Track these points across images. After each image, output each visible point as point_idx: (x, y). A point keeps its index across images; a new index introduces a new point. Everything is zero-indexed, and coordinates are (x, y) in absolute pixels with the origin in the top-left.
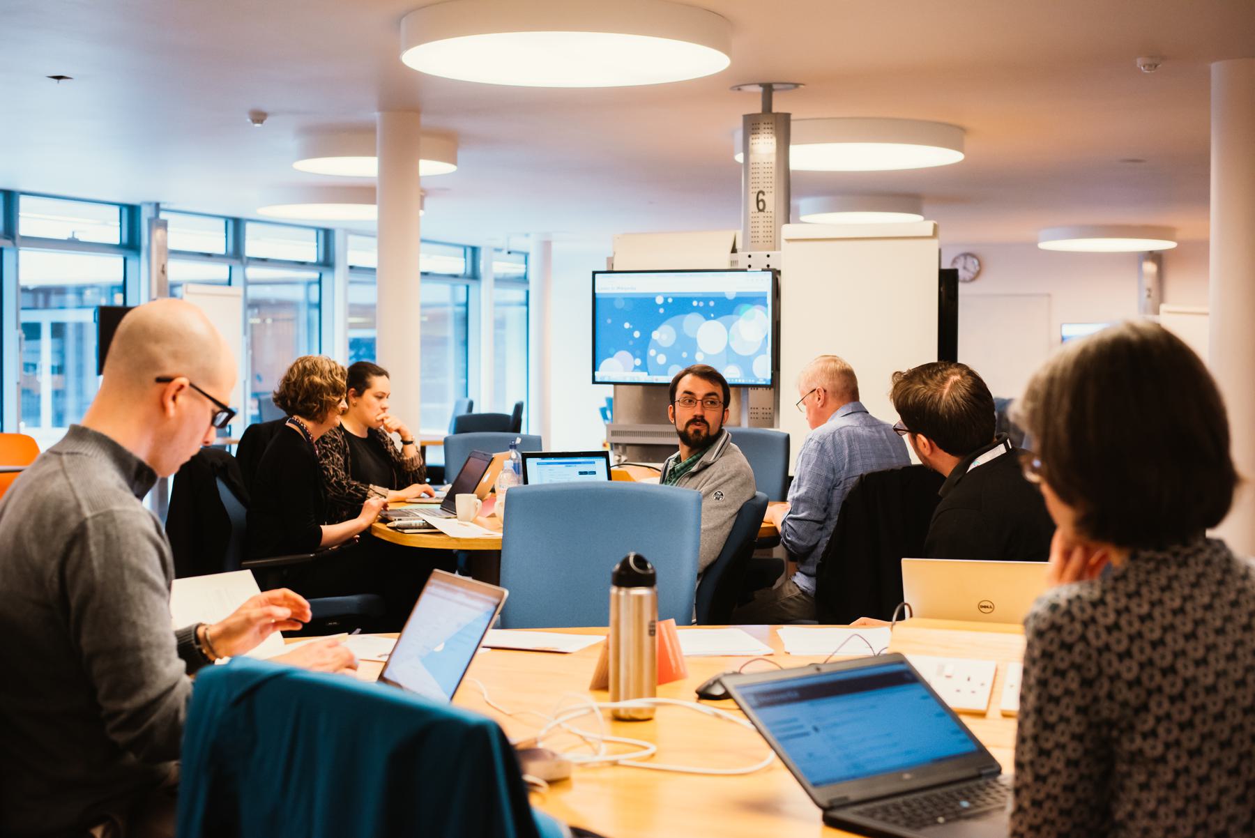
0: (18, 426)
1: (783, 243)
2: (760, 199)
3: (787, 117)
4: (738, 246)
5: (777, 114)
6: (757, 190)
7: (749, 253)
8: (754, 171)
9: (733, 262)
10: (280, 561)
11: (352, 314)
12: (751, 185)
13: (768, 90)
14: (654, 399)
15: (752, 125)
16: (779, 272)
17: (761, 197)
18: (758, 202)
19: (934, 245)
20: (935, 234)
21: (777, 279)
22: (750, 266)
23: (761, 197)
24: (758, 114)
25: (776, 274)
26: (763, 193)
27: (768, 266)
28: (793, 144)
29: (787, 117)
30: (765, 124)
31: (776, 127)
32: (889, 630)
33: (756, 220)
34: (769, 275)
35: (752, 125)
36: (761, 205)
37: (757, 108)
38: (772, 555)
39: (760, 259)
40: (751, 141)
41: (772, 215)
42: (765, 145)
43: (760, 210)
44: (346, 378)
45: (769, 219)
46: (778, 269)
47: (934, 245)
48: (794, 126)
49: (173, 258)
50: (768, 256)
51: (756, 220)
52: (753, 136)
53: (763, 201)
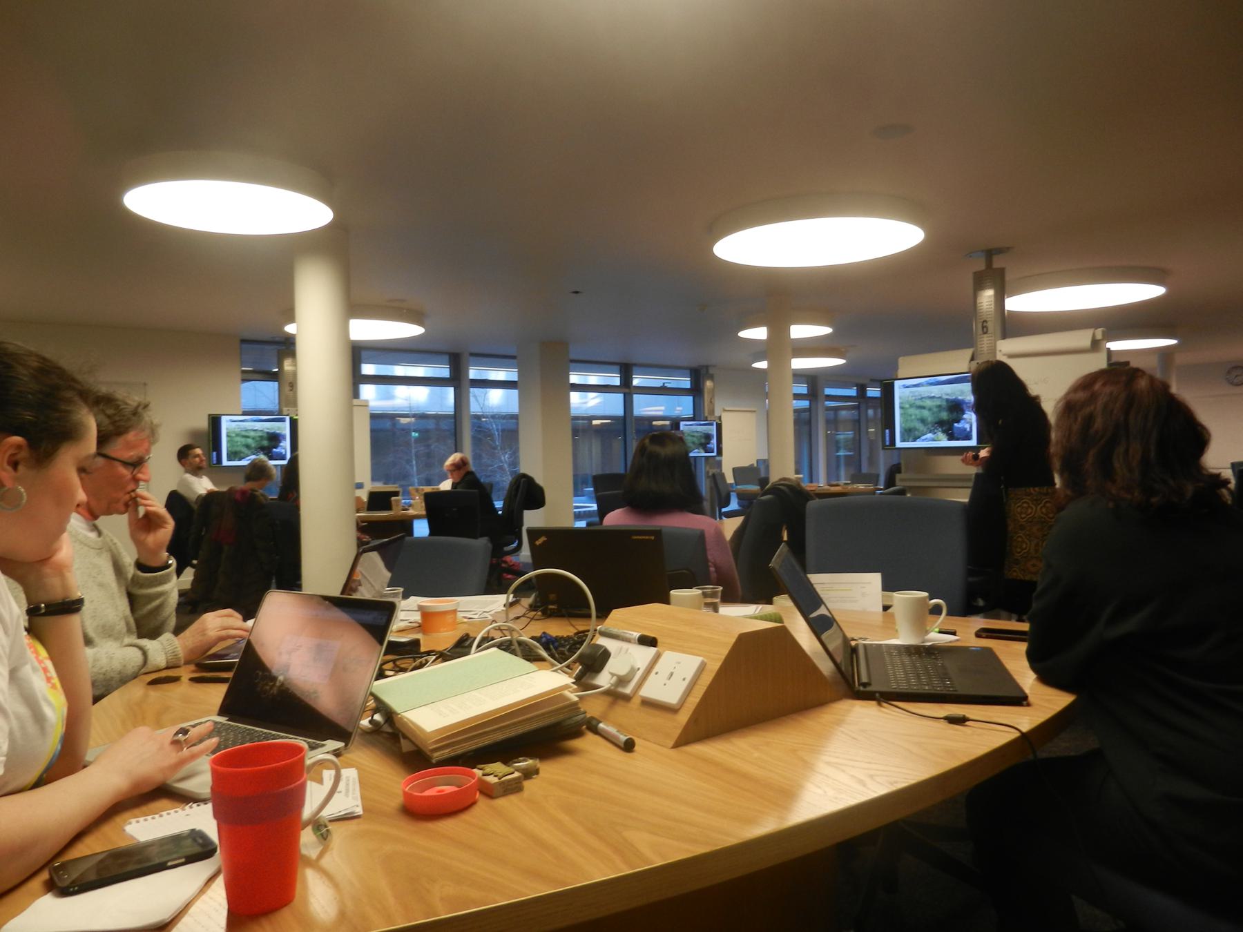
6: (982, 320)
35: (979, 284)
36: (985, 329)
53: (986, 327)
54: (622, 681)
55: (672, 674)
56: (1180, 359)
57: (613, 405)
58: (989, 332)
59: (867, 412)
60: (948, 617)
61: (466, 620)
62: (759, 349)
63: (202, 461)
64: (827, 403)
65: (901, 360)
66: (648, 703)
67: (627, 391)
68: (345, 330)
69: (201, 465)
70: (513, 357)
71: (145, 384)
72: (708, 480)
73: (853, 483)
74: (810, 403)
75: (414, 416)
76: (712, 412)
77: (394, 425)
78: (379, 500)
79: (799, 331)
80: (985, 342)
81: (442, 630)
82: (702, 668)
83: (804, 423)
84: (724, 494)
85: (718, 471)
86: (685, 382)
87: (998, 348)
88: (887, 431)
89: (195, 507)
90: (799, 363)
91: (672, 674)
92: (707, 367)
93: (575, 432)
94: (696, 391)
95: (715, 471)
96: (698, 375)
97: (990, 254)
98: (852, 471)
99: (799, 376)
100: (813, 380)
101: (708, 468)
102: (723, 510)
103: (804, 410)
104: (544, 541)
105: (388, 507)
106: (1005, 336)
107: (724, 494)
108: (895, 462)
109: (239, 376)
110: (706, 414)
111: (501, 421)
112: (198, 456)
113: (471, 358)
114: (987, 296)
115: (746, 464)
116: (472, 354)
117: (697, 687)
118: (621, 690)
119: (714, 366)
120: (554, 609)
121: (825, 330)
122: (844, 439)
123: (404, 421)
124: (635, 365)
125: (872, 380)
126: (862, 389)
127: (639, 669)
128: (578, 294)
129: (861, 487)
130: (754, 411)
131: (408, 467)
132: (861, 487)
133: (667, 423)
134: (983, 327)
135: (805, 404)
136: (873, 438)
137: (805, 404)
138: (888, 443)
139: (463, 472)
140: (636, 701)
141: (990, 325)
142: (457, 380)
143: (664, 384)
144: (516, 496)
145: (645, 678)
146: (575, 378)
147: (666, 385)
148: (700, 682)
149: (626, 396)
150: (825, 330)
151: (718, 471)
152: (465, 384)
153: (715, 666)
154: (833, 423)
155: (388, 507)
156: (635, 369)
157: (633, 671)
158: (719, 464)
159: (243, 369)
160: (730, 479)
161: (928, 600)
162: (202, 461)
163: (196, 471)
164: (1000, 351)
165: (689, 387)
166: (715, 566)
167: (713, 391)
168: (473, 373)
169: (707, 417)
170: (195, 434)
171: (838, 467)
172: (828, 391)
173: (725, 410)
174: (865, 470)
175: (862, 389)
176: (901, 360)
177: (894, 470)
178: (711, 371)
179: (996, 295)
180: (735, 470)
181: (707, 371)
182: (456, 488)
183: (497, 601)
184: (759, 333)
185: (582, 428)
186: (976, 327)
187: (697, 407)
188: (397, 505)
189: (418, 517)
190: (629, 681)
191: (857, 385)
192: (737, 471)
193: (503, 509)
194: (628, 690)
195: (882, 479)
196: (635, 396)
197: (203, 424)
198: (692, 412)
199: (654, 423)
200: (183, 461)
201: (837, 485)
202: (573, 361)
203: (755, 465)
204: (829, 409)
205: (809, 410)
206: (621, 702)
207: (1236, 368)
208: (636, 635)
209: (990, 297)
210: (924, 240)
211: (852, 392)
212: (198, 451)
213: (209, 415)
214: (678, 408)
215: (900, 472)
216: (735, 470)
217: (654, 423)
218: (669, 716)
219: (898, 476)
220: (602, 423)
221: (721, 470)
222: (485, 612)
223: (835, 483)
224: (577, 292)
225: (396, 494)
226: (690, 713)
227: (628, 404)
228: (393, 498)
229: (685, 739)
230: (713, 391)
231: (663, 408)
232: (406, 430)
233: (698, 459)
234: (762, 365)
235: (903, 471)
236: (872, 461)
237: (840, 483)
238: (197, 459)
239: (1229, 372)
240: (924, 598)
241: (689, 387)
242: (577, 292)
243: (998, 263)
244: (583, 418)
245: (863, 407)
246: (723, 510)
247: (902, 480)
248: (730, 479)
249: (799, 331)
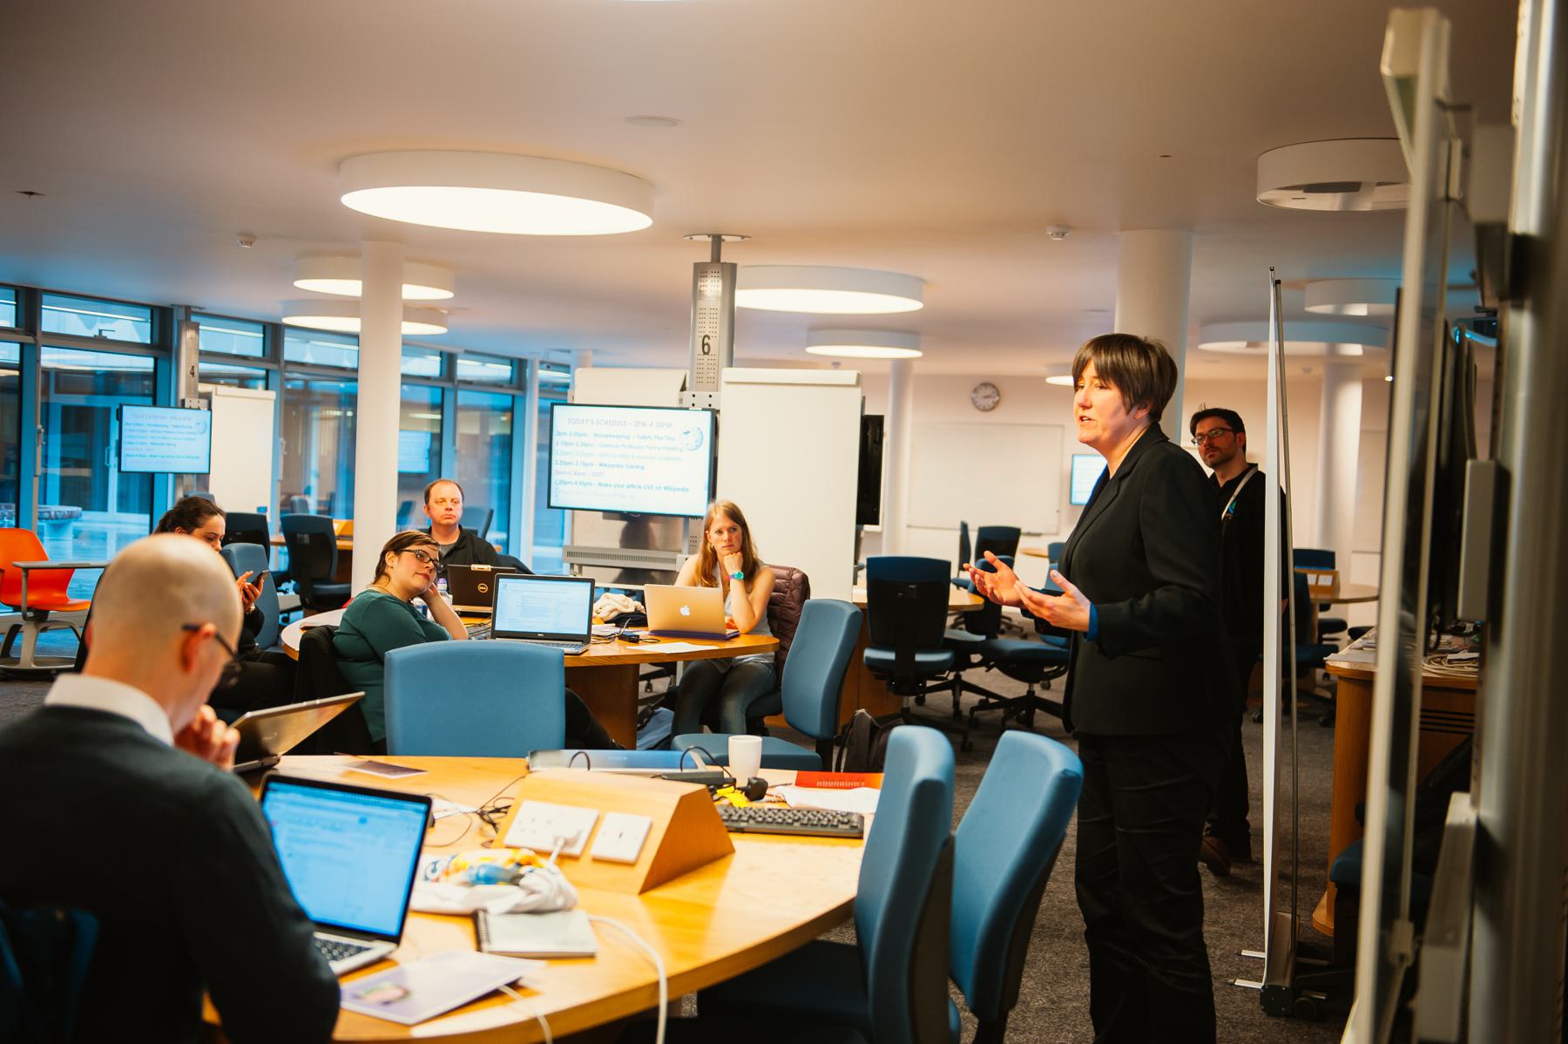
1: (723, 385)
2: (705, 342)
3: (734, 266)
4: (687, 385)
5: (725, 263)
6: (703, 335)
7: (693, 393)
9: (681, 401)
10: (341, 588)
11: (840, 771)
12: (698, 330)
13: (717, 240)
14: (685, 611)
15: (700, 271)
16: (718, 411)
18: (703, 345)
19: (858, 390)
20: (858, 383)
21: (716, 418)
22: (693, 405)
23: (706, 340)
24: (708, 263)
25: (715, 414)
26: (709, 338)
27: (710, 405)
28: (740, 289)
29: (734, 266)
31: (723, 275)
32: (475, 810)
33: (701, 362)
34: (709, 414)
36: (706, 348)
37: (708, 259)
38: (798, 775)
39: (703, 399)
40: (700, 284)
41: (715, 357)
42: (712, 287)
43: (705, 353)
44: (690, 667)
45: (713, 362)
46: (717, 409)
47: (857, 393)
48: (741, 274)
51: (701, 362)
52: (702, 279)
53: (708, 344)
56: (917, 369)
60: (388, 752)
67: (29, 339)
110: (182, 395)
125: (467, 352)
128: (32, 197)
140: (586, 860)
147: (104, 334)
149: (26, 348)
169: (183, 401)
194: (575, 850)
196: (43, 349)
205: (153, 376)
207: (985, 385)
210: (648, 228)
227: (29, 353)
229: (644, 890)
233: (156, 475)
239: (975, 391)
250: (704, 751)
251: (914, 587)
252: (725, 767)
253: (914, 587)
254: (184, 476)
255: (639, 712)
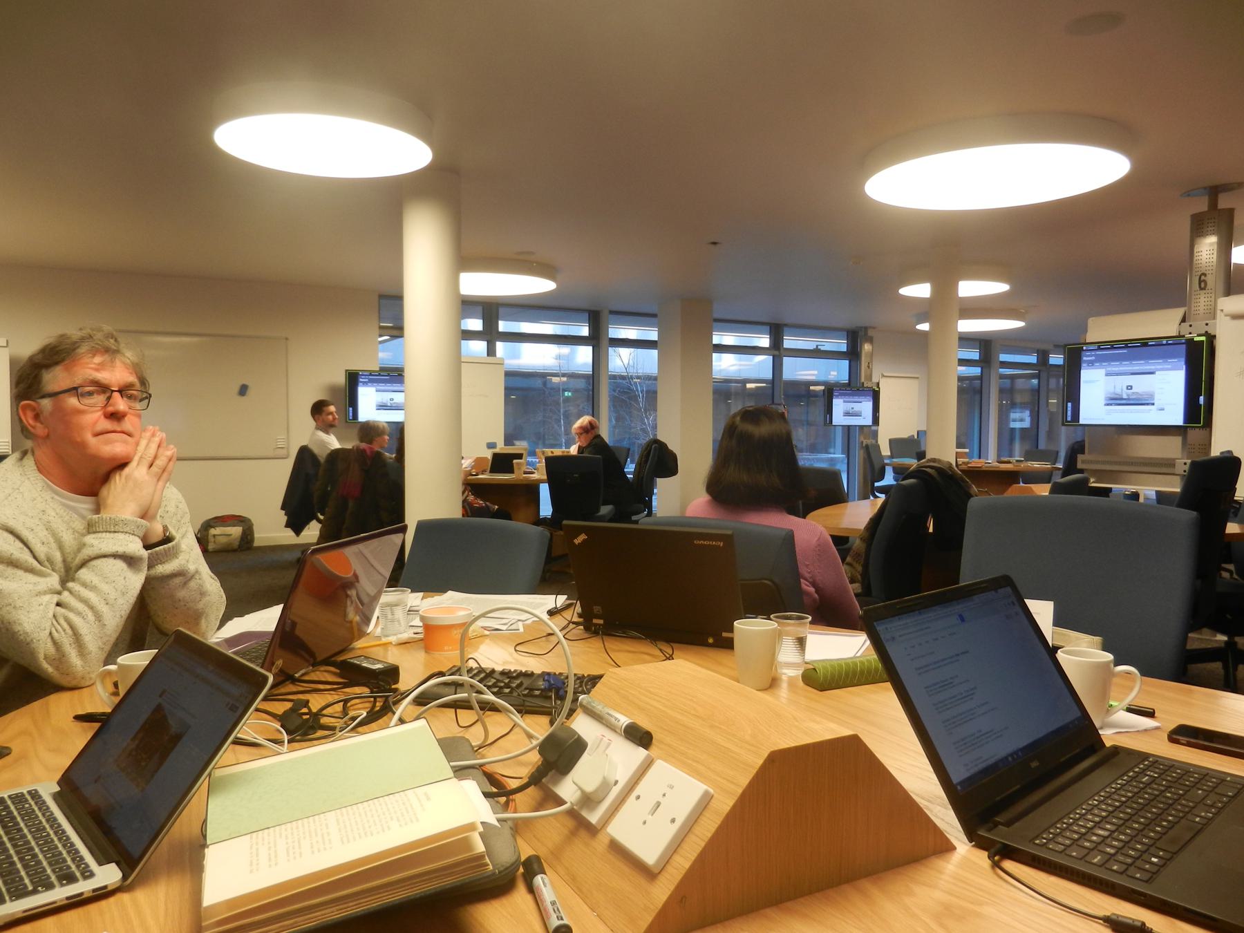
0: (516, 847)
2: (1202, 279)
6: (1200, 273)
8: (1196, 305)
17: (1203, 278)
23: (1203, 278)
24: (1206, 212)
30: (1208, 219)
35: (1199, 227)
36: (1203, 285)
46: (1212, 334)
49: (647, 864)
50: (1207, 324)
53: (1204, 281)
54: (589, 800)
55: (658, 804)
57: (759, 367)
58: (1208, 287)
59: (1048, 381)
61: (487, 633)
62: (924, 309)
63: (334, 419)
64: (1001, 370)
65: (1091, 321)
66: (617, 849)
67: (776, 353)
68: (455, 283)
69: (333, 423)
70: (654, 316)
71: (287, 339)
72: (862, 452)
73: (1027, 460)
74: (982, 371)
75: (564, 375)
76: (870, 378)
77: (545, 384)
78: (502, 462)
79: (969, 288)
80: (1201, 302)
81: (446, 648)
82: (705, 803)
83: (971, 393)
84: (877, 467)
85: (874, 442)
86: (841, 345)
87: (1220, 307)
88: (1069, 405)
89: (322, 460)
90: (967, 326)
91: (658, 804)
92: (866, 329)
93: (717, 392)
94: (853, 354)
95: (870, 441)
96: (855, 338)
97: (1214, 192)
98: (1027, 447)
99: (967, 340)
100: (985, 344)
101: (862, 439)
102: (877, 484)
103: (971, 379)
104: (584, 540)
105: (510, 470)
106: (1228, 292)
107: (877, 467)
108: (1079, 439)
109: (377, 331)
111: (647, 382)
112: (331, 413)
113: (611, 316)
114: (1207, 248)
115: (905, 435)
116: (612, 312)
117: (692, 838)
118: (585, 813)
119: (874, 328)
120: (600, 625)
121: (1000, 287)
122: (73, 871)
123: (555, 380)
124: (786, 325)
125: (1056, 346)
126: (1043, 356)
127: (616, 782)
129: (1036, 465)
130: (917, 378)
131: (556, 426)
132: (1036, 465)
133: (823, 388)
134: (1200, 282)
135: (976, 371)
136: (1053, 409)
137: (976, 371)
138: (1069, 419)
139: (590, 436)
140: (601, 842)
141: (1210, 280)
142: (596, 340)
143: (817, 346)
144: (646, 462)
145: (623, 800)
146: (717, 339)
147: (819, 347)
148: (697, 830)
150: (1000, 287)
151: (874, 442)
152: (605, 343)
153: (724, 804)
154: (1008, 393)
155: (510, 470)
156: (786, 329)
157: (606, 786)
158: (875, 434)
159: (381, 324)
160: (885, 451)
161: (1112, 665)
162: (334, 419)
163: (327, 427)
164: (1222, 310)
165: (845, 350)
166: (814, 584)
167: (871, 355)
168: (503, 326)
170: (333, 390)
171: (1012, 440)
172: (1004, 357)
173: (883, 376)
174: (1042, 445)
175: (1043, 356)
176: (1091, 321)
177: (1077, 449)
178: (870, 333)
179: (1219, 244)
180: (891, 441)
181: (866, 333)
182: (582, 453)
183: (546, 604)
184: (920, 290)
185: (725, 391)
186: (1192, 283)
187: (853, 371)
188: (519, 469)
189: (543, 481)
190: (600, 802)
191: (1038, 352)
192: (894, 443)
193: (634, 473)
194: (594, 818)
195: (1062, 455)
197: (341, 379)
198: (847, 378)
199: (812, 388)
200: (316, 416)
201: (1009, 462)
202: (716, 320)
203: (916, 437)
204: (1002, 377)
205: (981, 378)
206: (583, 833)
208: (624, 721)
209: (1211, 244)
211: (1032, 359)
212: (332, 408)
213: (346, 371)
214: (832, 373)
215: (1083, 452)
216: (891, 441)
217: (812, 388)
218: (642, 881)
219: (1080, 457)
220: (757, 388)
221: (877, 442)
222: (519, 620)
223: (1006, 459)
224: (715, 243)
225: (519, 456)
226: (672, 887)
227: (777, 367)
228: (515, 461)
230: (871, 355)
231: (816, 372)
232: (557, 390)
234: (924, 327)
235: (1086, 451)
236: (1051, 435)
237: (1012, 460)
238: (330, 417)
240: (1106, 664)
241: (845, 350)
242: (715, 243)
243: (1224, 202)
244: (737, 381)
245: (1044, 375)
246: (877, 484)
247: (1083, 462)
248: (885, 451)
249: (969, 288)
250: (476, 661)
251: (577, 475)
252: (402, 685)
253: (577, 475)
254: (865, 428)
255: (275, 612)
